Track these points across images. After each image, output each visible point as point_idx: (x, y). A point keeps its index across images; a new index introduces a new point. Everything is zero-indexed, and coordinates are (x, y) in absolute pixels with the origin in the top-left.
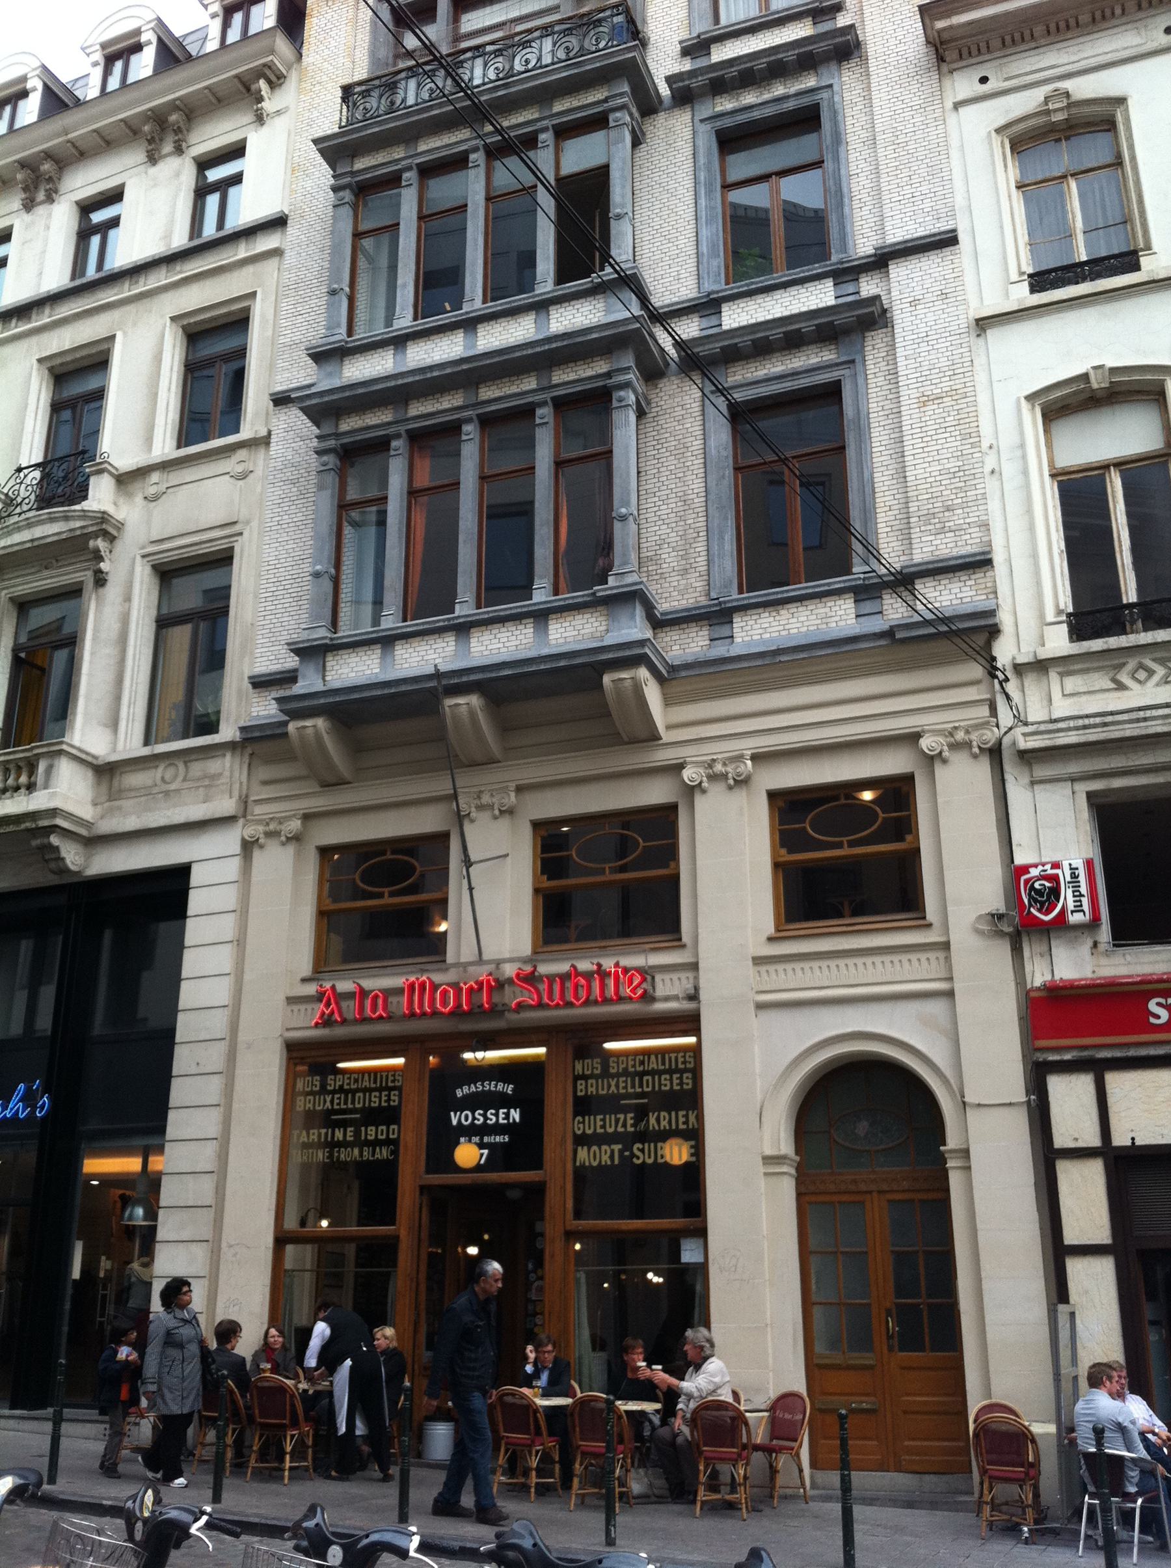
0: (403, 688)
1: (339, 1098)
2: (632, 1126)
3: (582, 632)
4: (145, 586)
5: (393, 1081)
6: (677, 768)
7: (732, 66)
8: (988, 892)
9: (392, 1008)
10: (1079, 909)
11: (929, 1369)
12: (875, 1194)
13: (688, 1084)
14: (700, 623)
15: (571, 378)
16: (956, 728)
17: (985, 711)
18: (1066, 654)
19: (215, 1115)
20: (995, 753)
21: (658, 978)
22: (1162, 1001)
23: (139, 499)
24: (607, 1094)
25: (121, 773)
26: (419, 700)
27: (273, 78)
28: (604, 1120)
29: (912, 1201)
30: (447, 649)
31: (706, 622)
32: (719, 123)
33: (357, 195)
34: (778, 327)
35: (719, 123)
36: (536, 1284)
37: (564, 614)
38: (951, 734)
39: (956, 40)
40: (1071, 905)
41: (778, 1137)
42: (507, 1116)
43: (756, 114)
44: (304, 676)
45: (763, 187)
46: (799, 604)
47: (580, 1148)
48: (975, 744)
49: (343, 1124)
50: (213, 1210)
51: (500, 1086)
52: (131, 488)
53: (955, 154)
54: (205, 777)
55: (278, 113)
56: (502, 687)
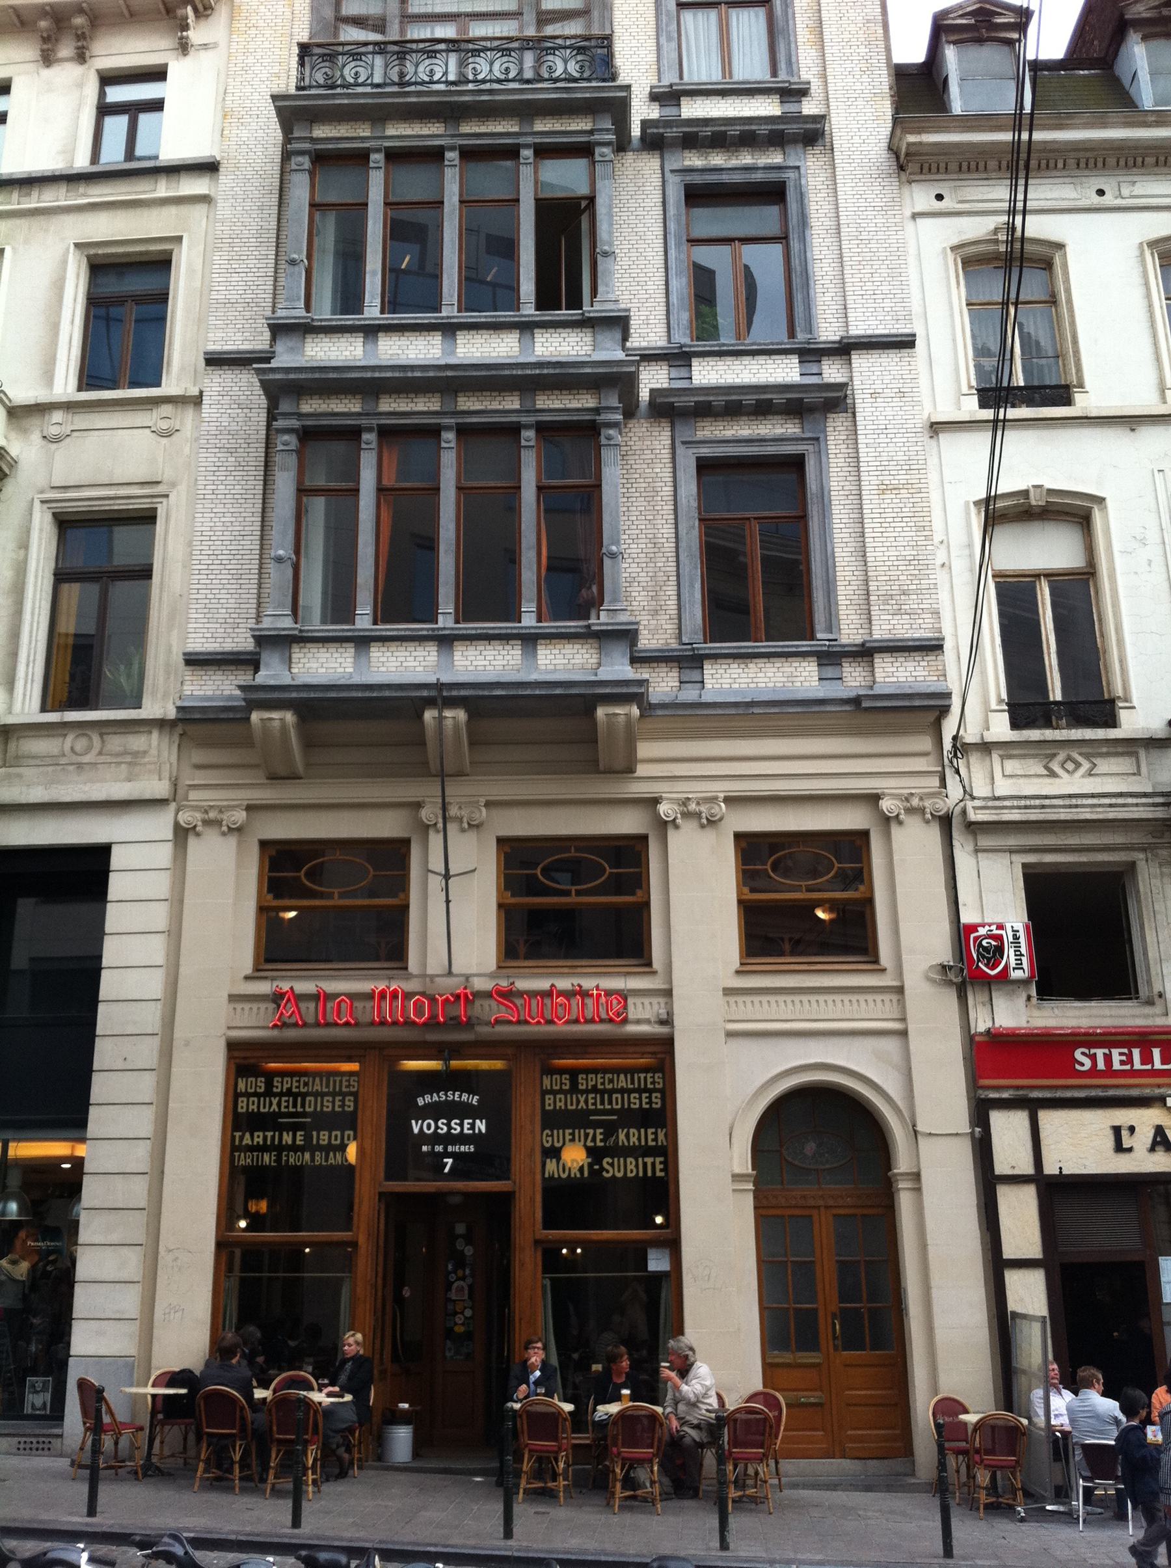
0: (387, 694)
1: (288, 1101)
2: (601, 1141)
3: (572, 661)
4: (44, 535)
5: (347, 1087)
6: (655, 801)
7: (707, 126)
8: (942, 950)
9: (359, 1014)
10: (1019, 967)
11: (866, 1366)
12: (822, 1209)
13: (657, 1104)
14: (670, 664)
15: (557, 406)
16: (912, 794)
17: (935, 782)
18: (1008, 740)
19: (149, 1114)
20: (945, 822)
21: (630, 1001)
22: (1087, 1051)
23: (36, 437)
24: (576, 1110)
25: (18, 739)
26: (400, 707)
27: (200, 7)
28: (573, 1134)
29: (855, 1215)
30: (428, 658)
31: (676, 664)
32: (688, 178)
33: (313, 162)
34: (752, 393)
35: (688, 178)
36: (455, 1285)
37: (553, 641)
38: (907, 800)
39: (921, 154)
40: (1013, 963)
41: (741, 1159)
42: (473, 1126)
43: (725, 178)
44: (267, 665)
45: (726, 249)
46: (766, 660)
47: (548, 1161)
48: (928, 810)
49: (294, 1128)
50: (145, 1213)
51: (465, 1097)
52: (26, 423)
53: (912, 260)
54: (125, 753)
55: (205, 46)
56: (487, 705)
